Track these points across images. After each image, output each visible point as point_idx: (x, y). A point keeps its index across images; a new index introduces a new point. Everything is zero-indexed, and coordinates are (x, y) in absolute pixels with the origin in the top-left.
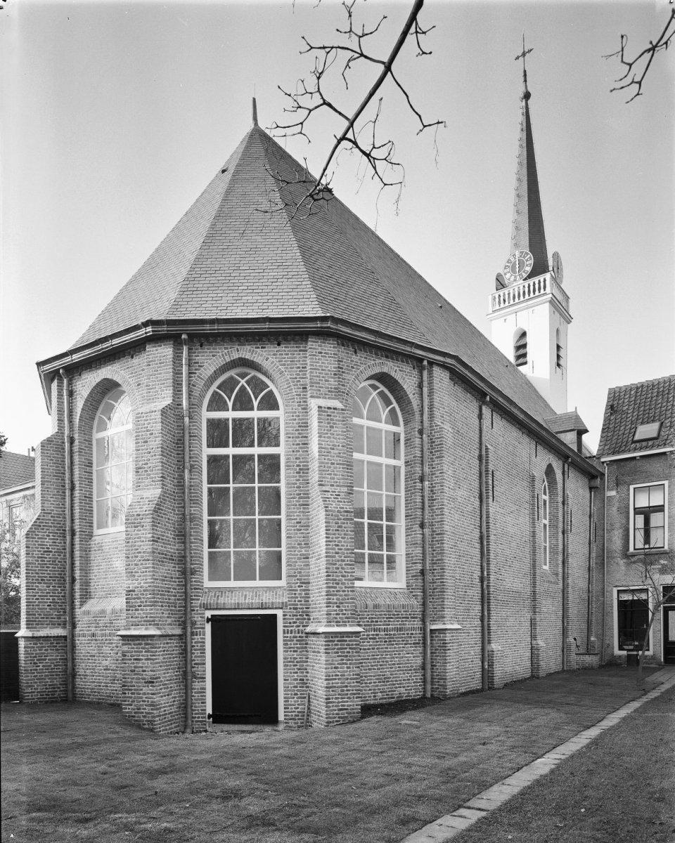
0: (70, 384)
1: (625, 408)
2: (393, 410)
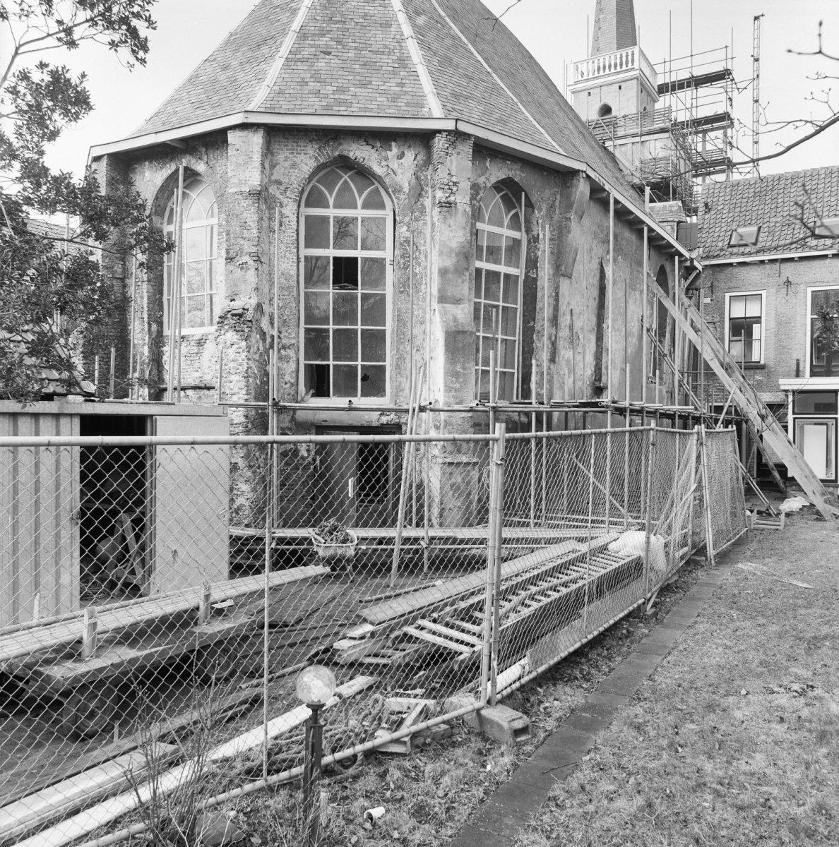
0: (346, 651)
1: (720, 208)
2: (516, 215)
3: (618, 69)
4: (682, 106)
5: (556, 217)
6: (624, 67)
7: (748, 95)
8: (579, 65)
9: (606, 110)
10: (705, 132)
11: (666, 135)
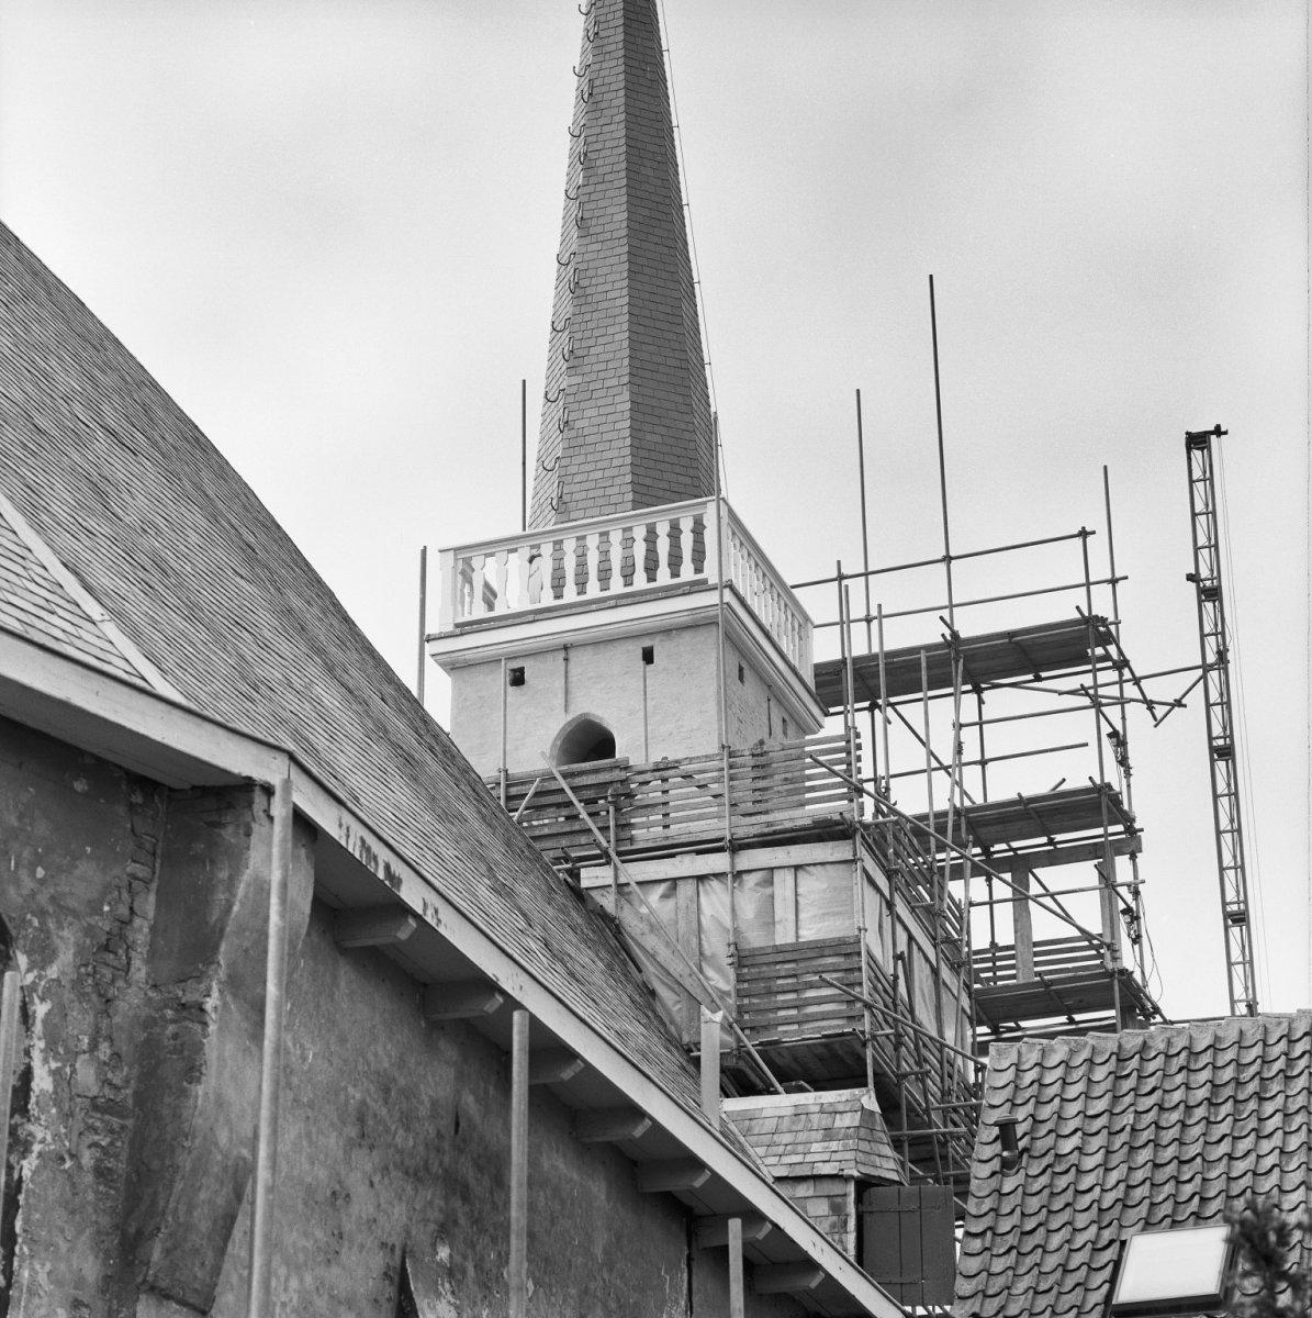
1: (1066, 1146)
3: (640, 582)
4: (916, 759)
5: (132, 1000)
6: (664, 577)
7: (1189, 728)
8: (476, 563)
9: (590, 742)
10: (1021, 867)
11: (840, 850)
